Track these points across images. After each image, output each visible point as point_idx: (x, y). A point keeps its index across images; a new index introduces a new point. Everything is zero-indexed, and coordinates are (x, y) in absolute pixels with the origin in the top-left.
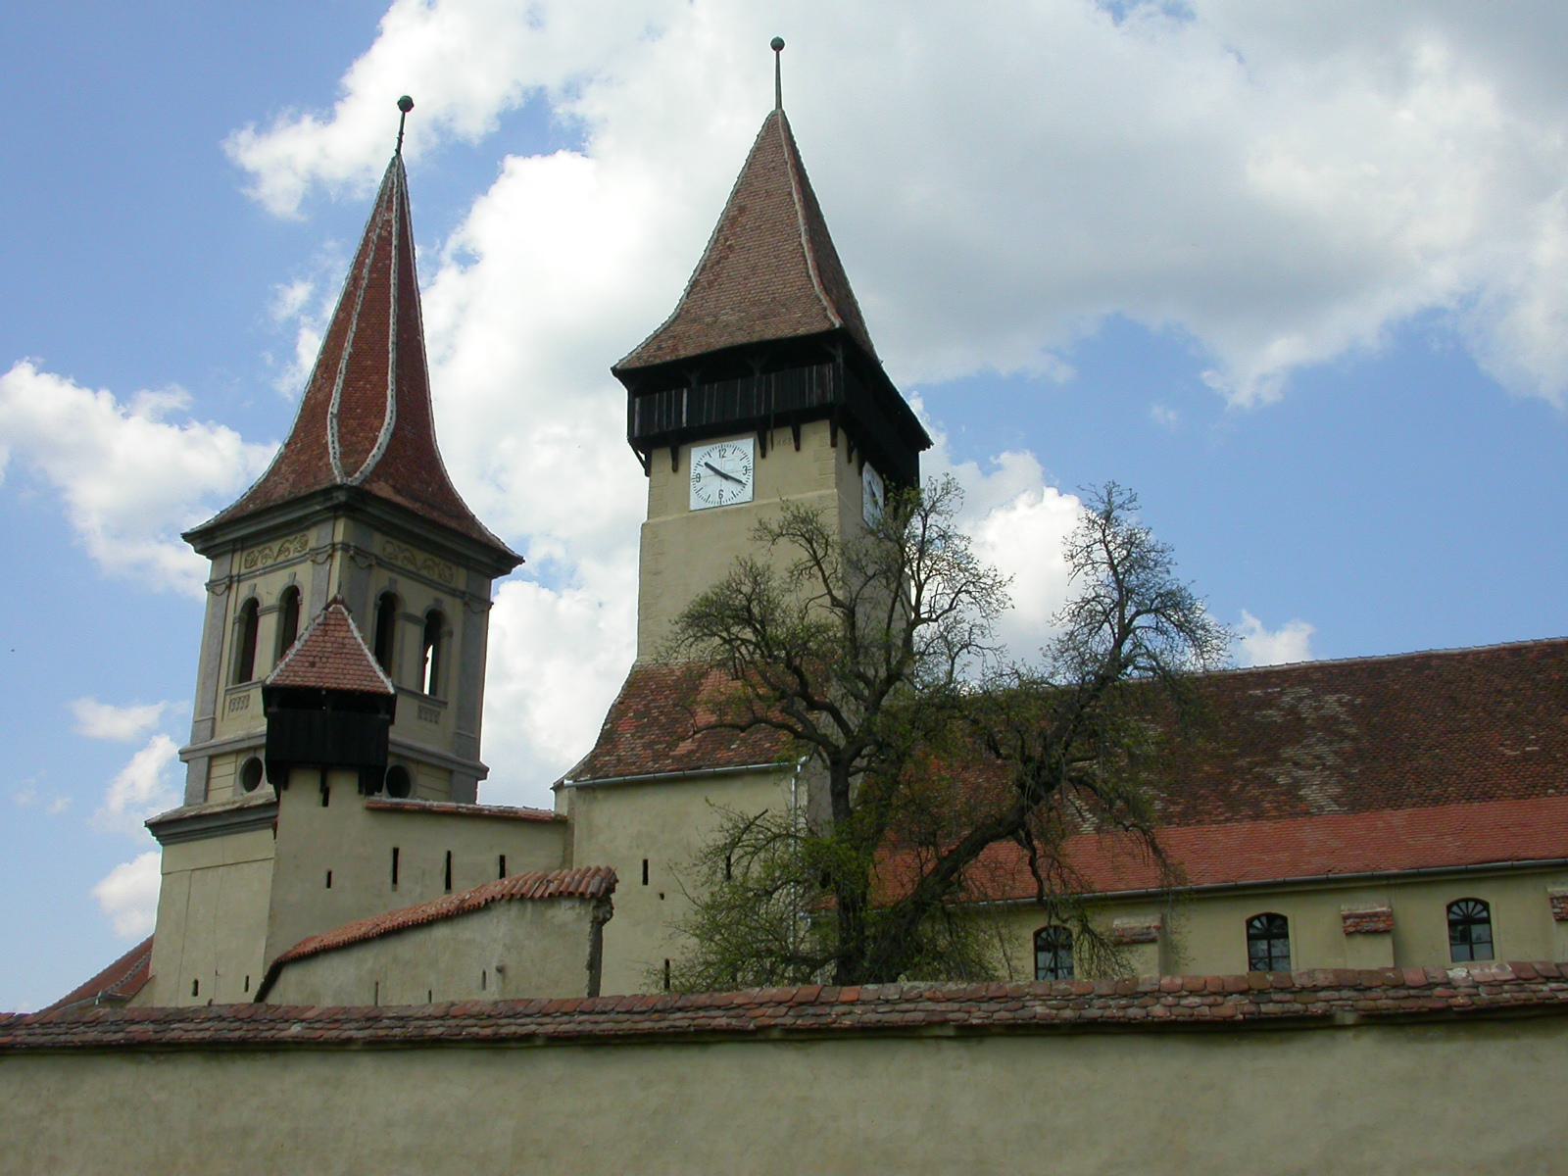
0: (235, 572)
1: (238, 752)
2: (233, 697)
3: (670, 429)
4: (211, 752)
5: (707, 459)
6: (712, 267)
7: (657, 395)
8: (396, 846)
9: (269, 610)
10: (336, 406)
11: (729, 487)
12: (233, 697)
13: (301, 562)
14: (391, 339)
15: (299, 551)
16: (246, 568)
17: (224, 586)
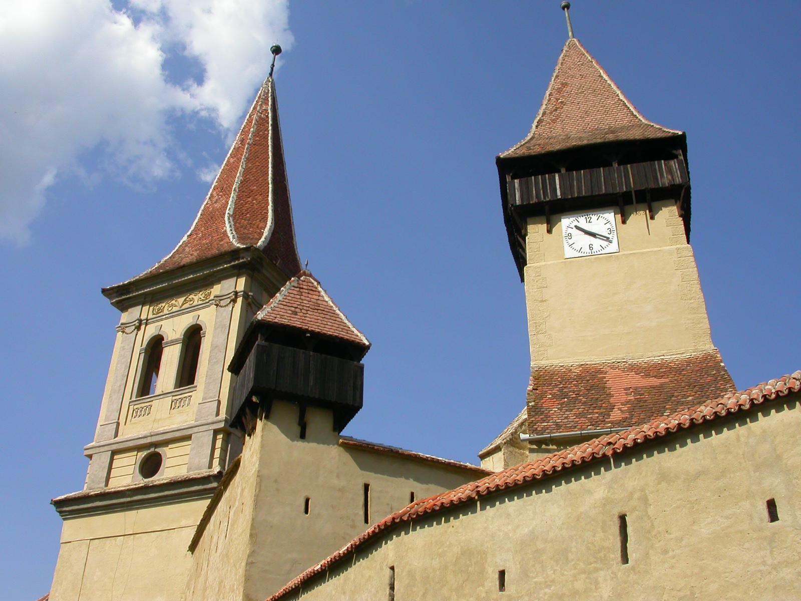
0: (143, 317)
1: (139, 448)
2: (136, 407)
3: (548, 199)
4: (114, 447)
5: (576, 223)
6: (551, 113)
7: (533, 178)
8: (367, 483)
9: (173, 342)
10: (232, 210)
11: (597, 243)
12: (136, 407)
13: (203, 308)
14: (270, 175)
15: (203, 300)
16: (154, 314)
17: (134, 327)
